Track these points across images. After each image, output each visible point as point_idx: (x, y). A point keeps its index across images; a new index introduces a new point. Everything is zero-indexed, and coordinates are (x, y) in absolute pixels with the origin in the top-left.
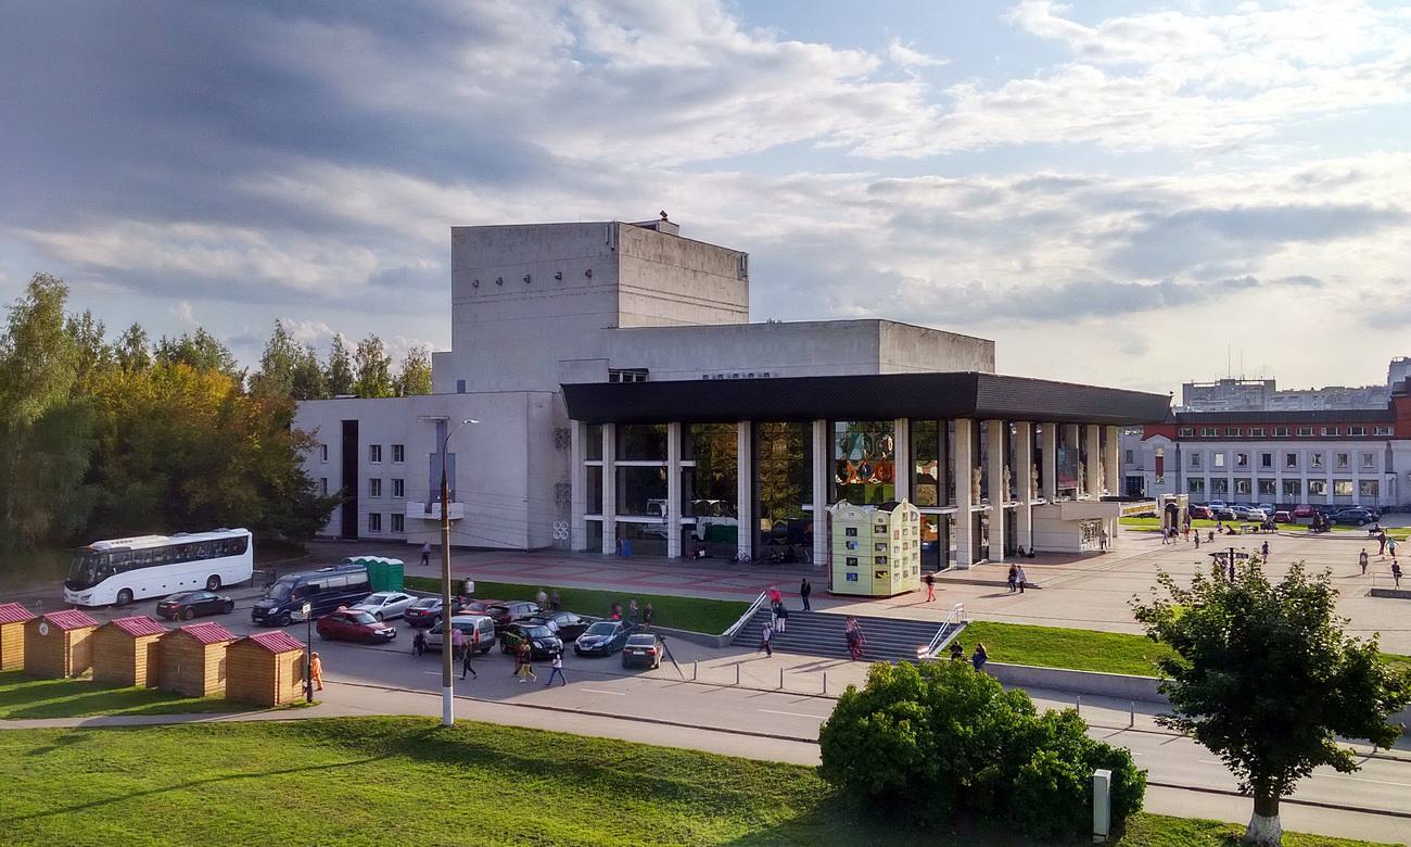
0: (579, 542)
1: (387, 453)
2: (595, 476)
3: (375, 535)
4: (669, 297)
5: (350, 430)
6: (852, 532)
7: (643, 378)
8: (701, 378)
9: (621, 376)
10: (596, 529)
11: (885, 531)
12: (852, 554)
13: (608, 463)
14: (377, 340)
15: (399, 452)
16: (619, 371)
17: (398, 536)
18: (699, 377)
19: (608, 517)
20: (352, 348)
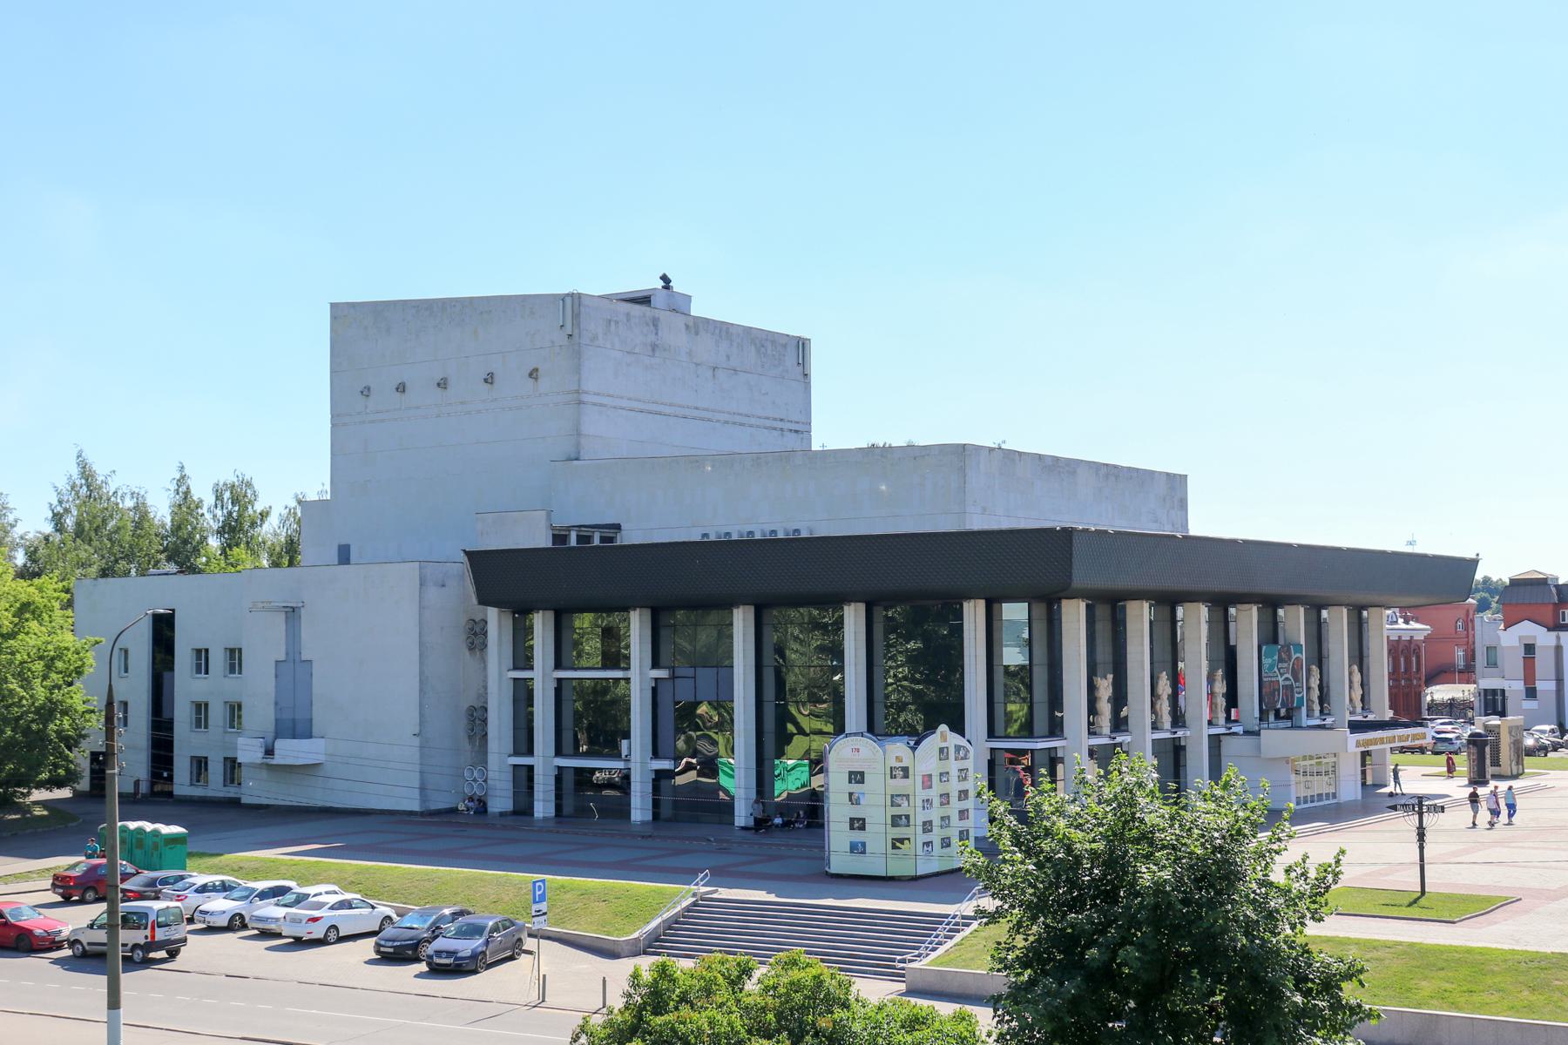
0: (500, 801)
1: (218, 660)
2: (523, 695)
3: (197, 792)
4: (667, 410)
5: (163, 628)
6: (857, 777)
7: (611, 540)
8: (698, 538)
9: (573, 536)
10: (524, 778)
11: (906, 776)
12: (857, 812)
13: (542, 676)
14: (249, 485)
15: (235, 658)
16: (569, 529)
17: (231, 792)
18: (695, 537)
19: (544, 761)
20: (203, 492)
